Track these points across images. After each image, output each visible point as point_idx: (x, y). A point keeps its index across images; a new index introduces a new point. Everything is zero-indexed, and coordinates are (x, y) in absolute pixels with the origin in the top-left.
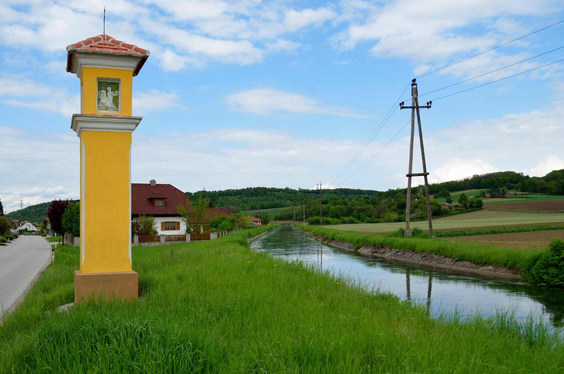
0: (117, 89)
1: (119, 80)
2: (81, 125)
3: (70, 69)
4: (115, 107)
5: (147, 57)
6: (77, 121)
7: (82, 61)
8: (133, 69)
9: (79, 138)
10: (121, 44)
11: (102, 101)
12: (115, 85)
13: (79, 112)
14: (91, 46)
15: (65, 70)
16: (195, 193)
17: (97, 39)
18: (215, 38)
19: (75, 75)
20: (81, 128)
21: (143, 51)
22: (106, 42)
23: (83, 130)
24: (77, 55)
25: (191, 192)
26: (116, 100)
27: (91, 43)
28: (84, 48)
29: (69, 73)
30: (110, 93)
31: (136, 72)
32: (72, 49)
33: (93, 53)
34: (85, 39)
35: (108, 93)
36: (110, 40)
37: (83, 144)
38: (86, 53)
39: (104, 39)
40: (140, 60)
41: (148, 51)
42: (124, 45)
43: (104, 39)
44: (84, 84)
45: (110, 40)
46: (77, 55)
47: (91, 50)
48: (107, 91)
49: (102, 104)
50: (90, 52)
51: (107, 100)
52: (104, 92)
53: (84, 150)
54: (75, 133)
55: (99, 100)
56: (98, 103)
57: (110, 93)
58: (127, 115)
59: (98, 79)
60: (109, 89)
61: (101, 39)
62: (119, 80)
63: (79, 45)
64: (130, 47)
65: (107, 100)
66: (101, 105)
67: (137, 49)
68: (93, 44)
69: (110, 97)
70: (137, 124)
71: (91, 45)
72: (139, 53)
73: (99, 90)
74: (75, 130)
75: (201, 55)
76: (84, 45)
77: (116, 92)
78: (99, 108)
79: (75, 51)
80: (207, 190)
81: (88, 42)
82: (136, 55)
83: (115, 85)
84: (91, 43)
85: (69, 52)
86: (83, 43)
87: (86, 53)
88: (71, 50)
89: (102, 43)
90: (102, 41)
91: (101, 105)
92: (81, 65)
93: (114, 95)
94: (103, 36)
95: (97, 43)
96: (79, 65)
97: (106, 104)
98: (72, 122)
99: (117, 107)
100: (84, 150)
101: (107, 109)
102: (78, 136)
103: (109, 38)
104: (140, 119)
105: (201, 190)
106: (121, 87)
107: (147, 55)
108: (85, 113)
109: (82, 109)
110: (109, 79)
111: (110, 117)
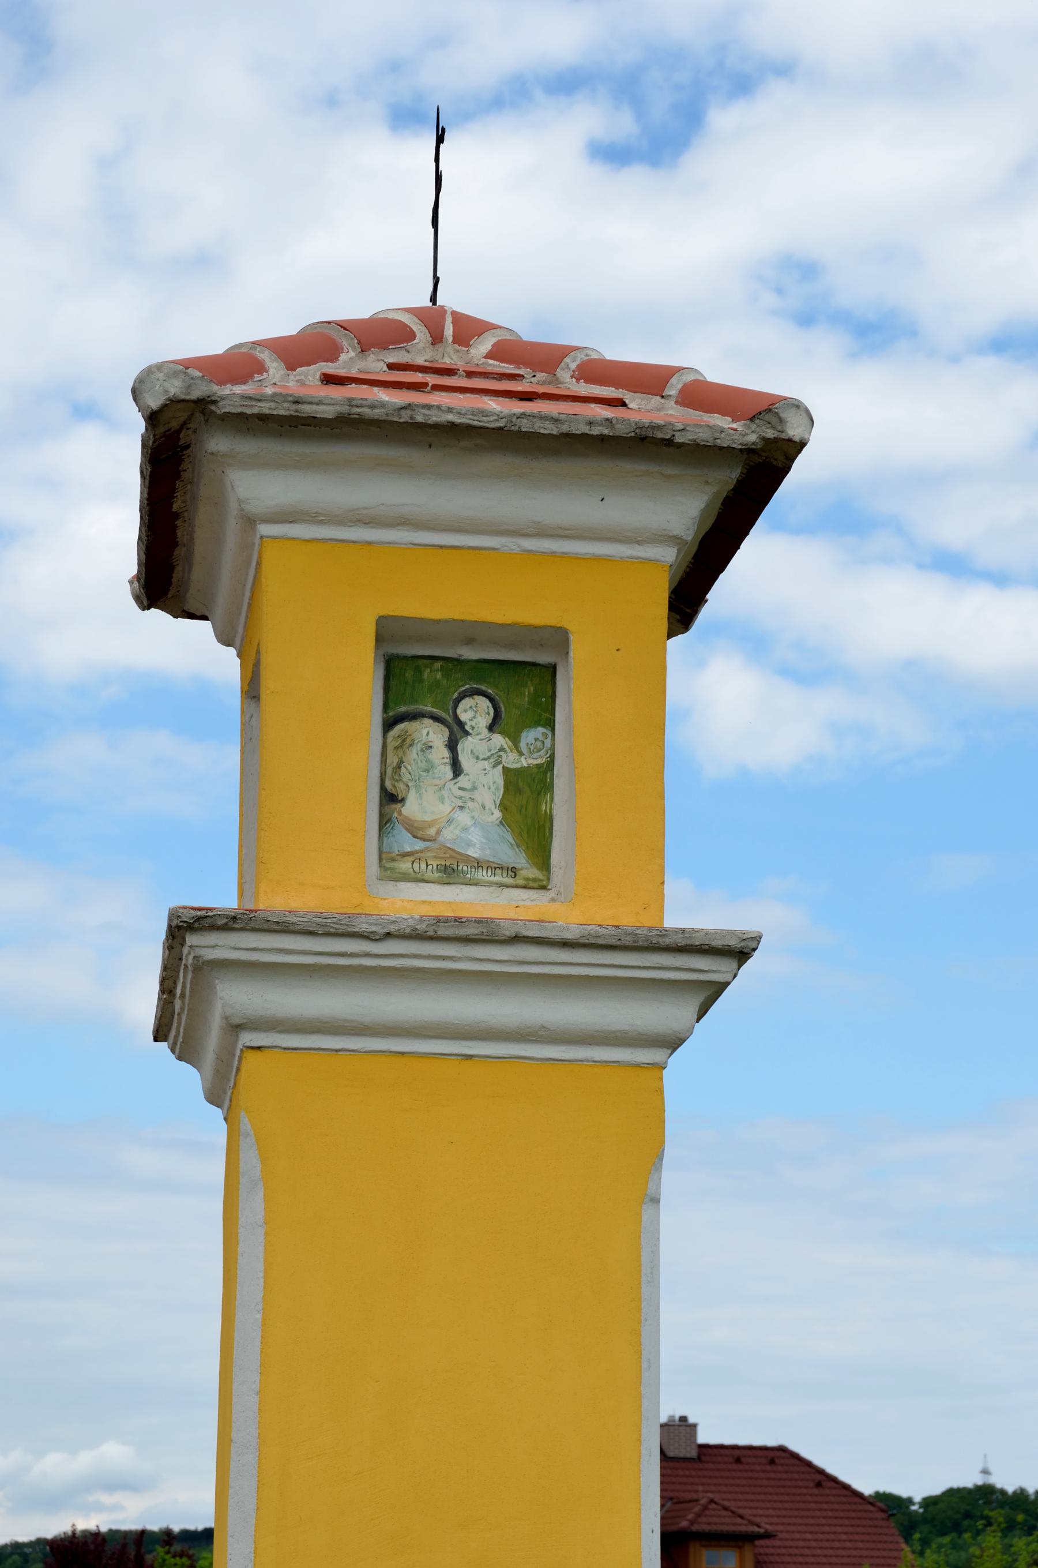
0: (544, 714)
1: (558, 639)
2: (234, 996)
3: (163, 579)
4: (519, 859)
5: (802, 445)
6: (204, 968)
7: (253, 485)
8: (669, 555)
9: (217, 1113)
10: (572, 363)
11: (412, 808)
12: (522, 678)
13: (222, 896)
14: (329, 379)
15: (151, 1036)
16: (929, 1502)
17: (378, 334)
18: (1000, 579)
19: (204, 629)
20: (235, 1028)
21: (766, 409)
22: (450, 356)
23: (248, 1038)
24: (218, 443)
25: (901, 1490)
26: (528, 799)
27: (333, 357)
28: (277, 381)
29: (156, 614)
30: (480, 744)
31: (685, 603)
32: (175, 388)
33: (351, 427)
34: (289, 328)
35: (465, 746)
36: (482, 346)
37: (250, 1159)
38: (291, 426)
39: (437, 338)
40: (730, 476)
41: (796, 405)
42: (596, 371)
43: (437, 338)
44: (269, 684)
45: (482, 346)
46: (218, 443)
47: (331, 401)
48: (457, 732)
49: (415, 830)
50: (327, 412)
51: (460, 799)
52: (431, 734)
53: (253, 1207)
54: (189, 1080)
55: (390, 798)
56: (385, 822)
57: (480, 744)
58: (625, 916)
59: (387, 630)
60: (475, 712)
61: (412, 336)
62: (558, 639)
63: (240, 364)
64: (651, 380)
65: (460, 799)
66: (409, 844)
67: (701, 395)
68: (348, 362)
69: (485, 781)
70: (712, 992)
71: (330, 368)
72: (723, 422)
73: (389, 725)
74: (186, 1053)
75: (921, 681)
76: (275, 370)
77: (531, 736)
78: (388, 865)
79: (203, 406)
80: (1007, 1482)
81: (296, 351)
82: (704, 436)
83: (522, 678)
84: (332, 353)
85: (152, 418)
86: (265, 356)
87: (291, 426)
88: (173, 403)
89: (420, 361)
90: (420, 352)
91: (409, 844)
92: (250, 522)
93: (511, 760)
94: (432, 317)
95: (375, 365)
96: (232, 529)
97: (448, 835)
98: (167, 987)
99: (541, 855)
100: (253, 1207)
101: (452, 871)
102: (215, 1096)
103: (468, 329)
104: (740, 952)
105: (969, 1479)
106: (577, 696)
107: (794, 432)
108: (274, 901)
109: (239, 903)
110: (471, 632)
111: (486, 934)
